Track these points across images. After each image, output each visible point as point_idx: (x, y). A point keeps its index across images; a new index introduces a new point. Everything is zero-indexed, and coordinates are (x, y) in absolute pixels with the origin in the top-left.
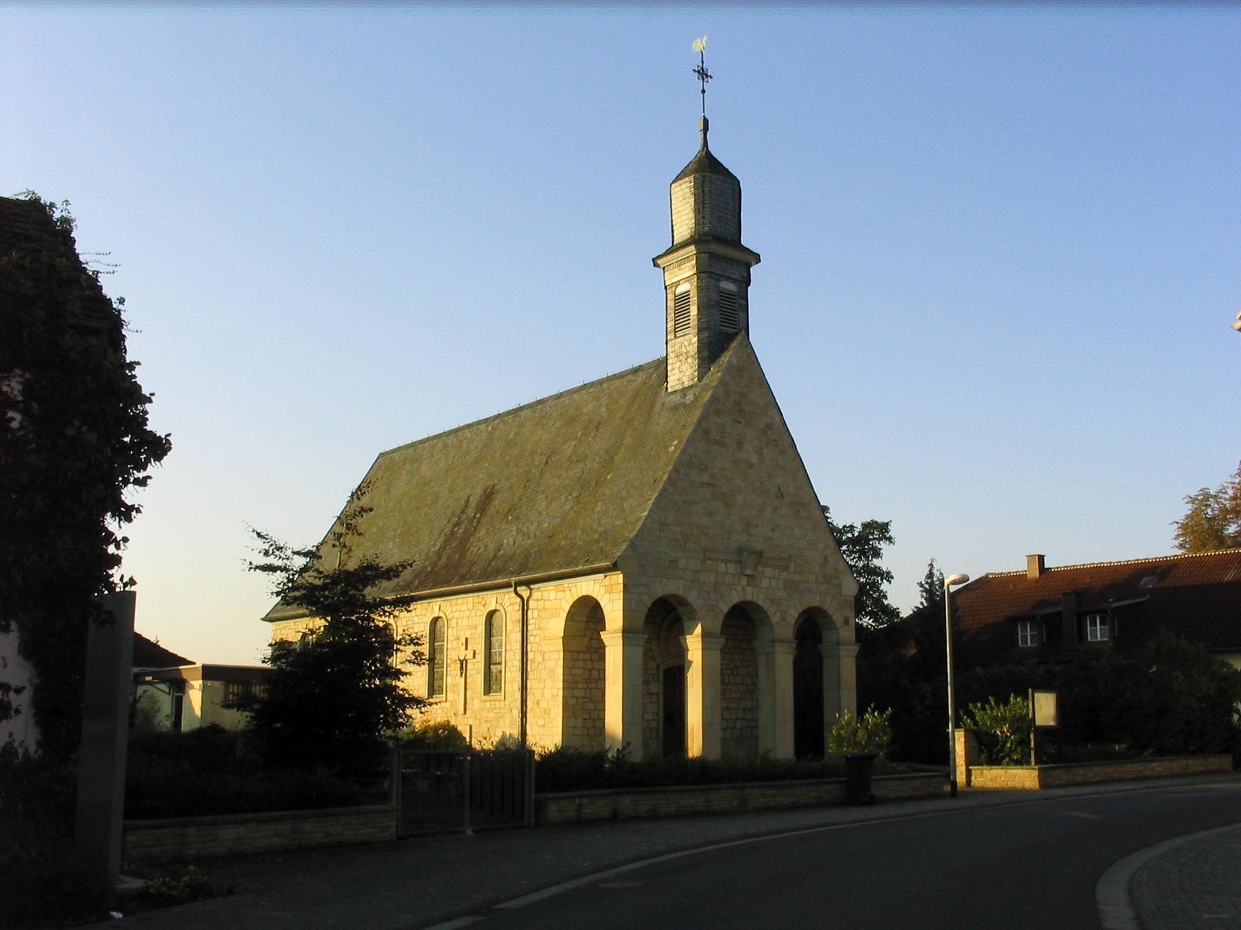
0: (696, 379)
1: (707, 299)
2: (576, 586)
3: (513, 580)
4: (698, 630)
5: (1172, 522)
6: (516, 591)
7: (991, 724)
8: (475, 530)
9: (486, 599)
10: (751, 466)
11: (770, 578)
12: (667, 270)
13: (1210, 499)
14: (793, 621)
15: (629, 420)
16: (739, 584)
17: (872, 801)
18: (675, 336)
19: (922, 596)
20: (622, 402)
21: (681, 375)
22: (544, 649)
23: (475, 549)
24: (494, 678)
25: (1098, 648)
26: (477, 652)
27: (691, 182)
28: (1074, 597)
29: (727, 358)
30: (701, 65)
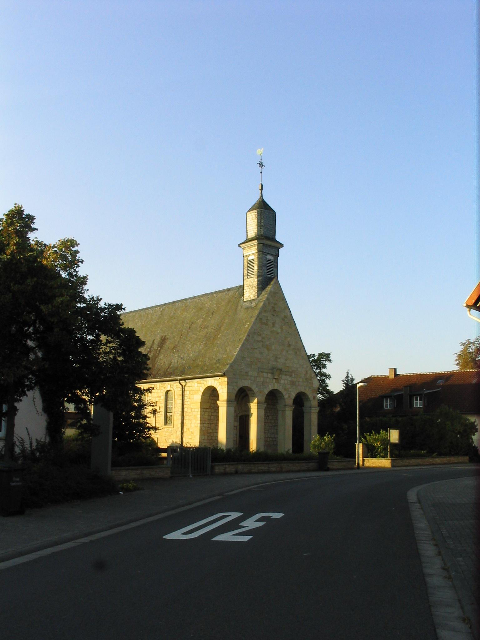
0: (256, 297)
1: (261, 263)
2: (206, 382)
3: (179, 378)
4: (256, 401)
5: (454, 353)
6: (180, 383)
7: (373, 442)
8: (158, 355)
9: (165, 385)
10: (278, 333)
11: (284, 380)
12: (245, 249)
13: (471, 344)
14: (293, 398)
15: (227, 312)
16: (272, 382)
17: (328, 470)
18: (247, 278)
19: (344, 386)
20: (223, 303)
21: (250, 294)
22: (192, 407)
23: (159, 364)
24: (169, 418)
25: (416, 412)
26: (161, 407)
27: (256, 213)
28: (408, 388)
29: (269, 289)
30: (260, 161)
